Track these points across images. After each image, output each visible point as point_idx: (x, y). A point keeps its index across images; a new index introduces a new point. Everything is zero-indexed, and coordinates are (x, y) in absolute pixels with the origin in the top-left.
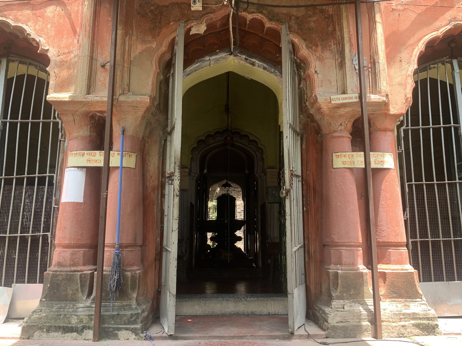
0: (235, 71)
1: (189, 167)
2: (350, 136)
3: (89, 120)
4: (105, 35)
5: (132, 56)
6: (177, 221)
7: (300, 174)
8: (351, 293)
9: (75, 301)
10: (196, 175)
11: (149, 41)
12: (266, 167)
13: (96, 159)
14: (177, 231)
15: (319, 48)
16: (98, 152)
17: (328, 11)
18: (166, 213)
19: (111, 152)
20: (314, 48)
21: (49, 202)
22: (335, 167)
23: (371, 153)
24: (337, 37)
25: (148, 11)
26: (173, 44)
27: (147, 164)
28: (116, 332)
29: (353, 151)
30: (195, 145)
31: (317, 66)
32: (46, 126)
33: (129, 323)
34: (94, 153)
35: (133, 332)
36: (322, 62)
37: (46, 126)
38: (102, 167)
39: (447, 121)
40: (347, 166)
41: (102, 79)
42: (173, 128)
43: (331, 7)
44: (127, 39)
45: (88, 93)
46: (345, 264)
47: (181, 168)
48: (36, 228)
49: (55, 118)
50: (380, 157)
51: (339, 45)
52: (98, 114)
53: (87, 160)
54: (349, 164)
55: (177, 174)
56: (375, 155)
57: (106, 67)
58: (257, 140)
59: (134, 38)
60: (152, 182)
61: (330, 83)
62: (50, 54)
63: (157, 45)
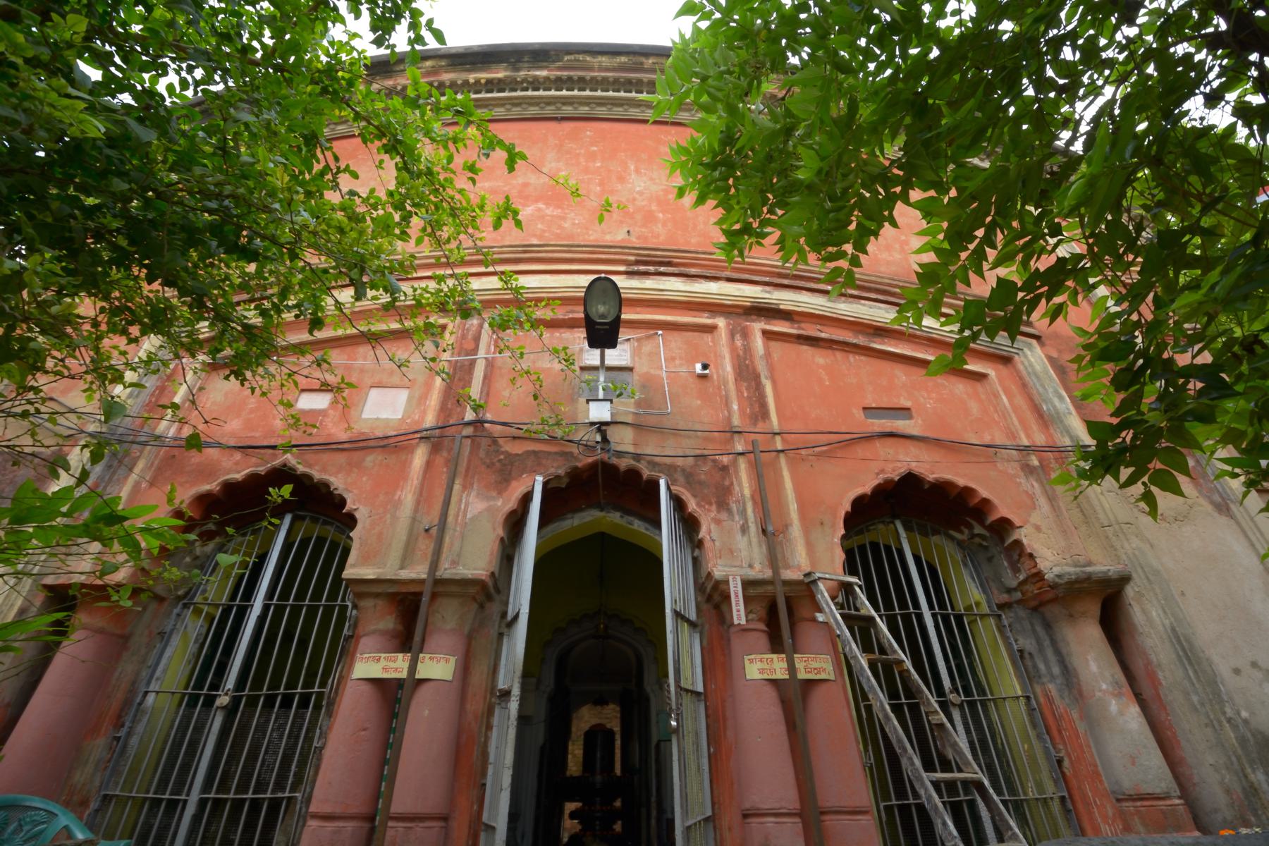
6: (511, 772)
7: (700, 688)
13: (395, 666)
15: (714, 507)
16: (400, 656)
18: (492, 758)
21: (309, 739)
22: (748, 677)
26: (527, 499)
29: (774, 652)
32: (329, 611)
37: (329, 611)
39: (903, 605)
40: (766, 676)
41: (423, 547)
42: (516, 617)
45: (402, 568)
48: (280, 786)
49: (343, 600)
55: (516, 691)
59: (473, 494)
60: (475, 705)
62: (357, 515)
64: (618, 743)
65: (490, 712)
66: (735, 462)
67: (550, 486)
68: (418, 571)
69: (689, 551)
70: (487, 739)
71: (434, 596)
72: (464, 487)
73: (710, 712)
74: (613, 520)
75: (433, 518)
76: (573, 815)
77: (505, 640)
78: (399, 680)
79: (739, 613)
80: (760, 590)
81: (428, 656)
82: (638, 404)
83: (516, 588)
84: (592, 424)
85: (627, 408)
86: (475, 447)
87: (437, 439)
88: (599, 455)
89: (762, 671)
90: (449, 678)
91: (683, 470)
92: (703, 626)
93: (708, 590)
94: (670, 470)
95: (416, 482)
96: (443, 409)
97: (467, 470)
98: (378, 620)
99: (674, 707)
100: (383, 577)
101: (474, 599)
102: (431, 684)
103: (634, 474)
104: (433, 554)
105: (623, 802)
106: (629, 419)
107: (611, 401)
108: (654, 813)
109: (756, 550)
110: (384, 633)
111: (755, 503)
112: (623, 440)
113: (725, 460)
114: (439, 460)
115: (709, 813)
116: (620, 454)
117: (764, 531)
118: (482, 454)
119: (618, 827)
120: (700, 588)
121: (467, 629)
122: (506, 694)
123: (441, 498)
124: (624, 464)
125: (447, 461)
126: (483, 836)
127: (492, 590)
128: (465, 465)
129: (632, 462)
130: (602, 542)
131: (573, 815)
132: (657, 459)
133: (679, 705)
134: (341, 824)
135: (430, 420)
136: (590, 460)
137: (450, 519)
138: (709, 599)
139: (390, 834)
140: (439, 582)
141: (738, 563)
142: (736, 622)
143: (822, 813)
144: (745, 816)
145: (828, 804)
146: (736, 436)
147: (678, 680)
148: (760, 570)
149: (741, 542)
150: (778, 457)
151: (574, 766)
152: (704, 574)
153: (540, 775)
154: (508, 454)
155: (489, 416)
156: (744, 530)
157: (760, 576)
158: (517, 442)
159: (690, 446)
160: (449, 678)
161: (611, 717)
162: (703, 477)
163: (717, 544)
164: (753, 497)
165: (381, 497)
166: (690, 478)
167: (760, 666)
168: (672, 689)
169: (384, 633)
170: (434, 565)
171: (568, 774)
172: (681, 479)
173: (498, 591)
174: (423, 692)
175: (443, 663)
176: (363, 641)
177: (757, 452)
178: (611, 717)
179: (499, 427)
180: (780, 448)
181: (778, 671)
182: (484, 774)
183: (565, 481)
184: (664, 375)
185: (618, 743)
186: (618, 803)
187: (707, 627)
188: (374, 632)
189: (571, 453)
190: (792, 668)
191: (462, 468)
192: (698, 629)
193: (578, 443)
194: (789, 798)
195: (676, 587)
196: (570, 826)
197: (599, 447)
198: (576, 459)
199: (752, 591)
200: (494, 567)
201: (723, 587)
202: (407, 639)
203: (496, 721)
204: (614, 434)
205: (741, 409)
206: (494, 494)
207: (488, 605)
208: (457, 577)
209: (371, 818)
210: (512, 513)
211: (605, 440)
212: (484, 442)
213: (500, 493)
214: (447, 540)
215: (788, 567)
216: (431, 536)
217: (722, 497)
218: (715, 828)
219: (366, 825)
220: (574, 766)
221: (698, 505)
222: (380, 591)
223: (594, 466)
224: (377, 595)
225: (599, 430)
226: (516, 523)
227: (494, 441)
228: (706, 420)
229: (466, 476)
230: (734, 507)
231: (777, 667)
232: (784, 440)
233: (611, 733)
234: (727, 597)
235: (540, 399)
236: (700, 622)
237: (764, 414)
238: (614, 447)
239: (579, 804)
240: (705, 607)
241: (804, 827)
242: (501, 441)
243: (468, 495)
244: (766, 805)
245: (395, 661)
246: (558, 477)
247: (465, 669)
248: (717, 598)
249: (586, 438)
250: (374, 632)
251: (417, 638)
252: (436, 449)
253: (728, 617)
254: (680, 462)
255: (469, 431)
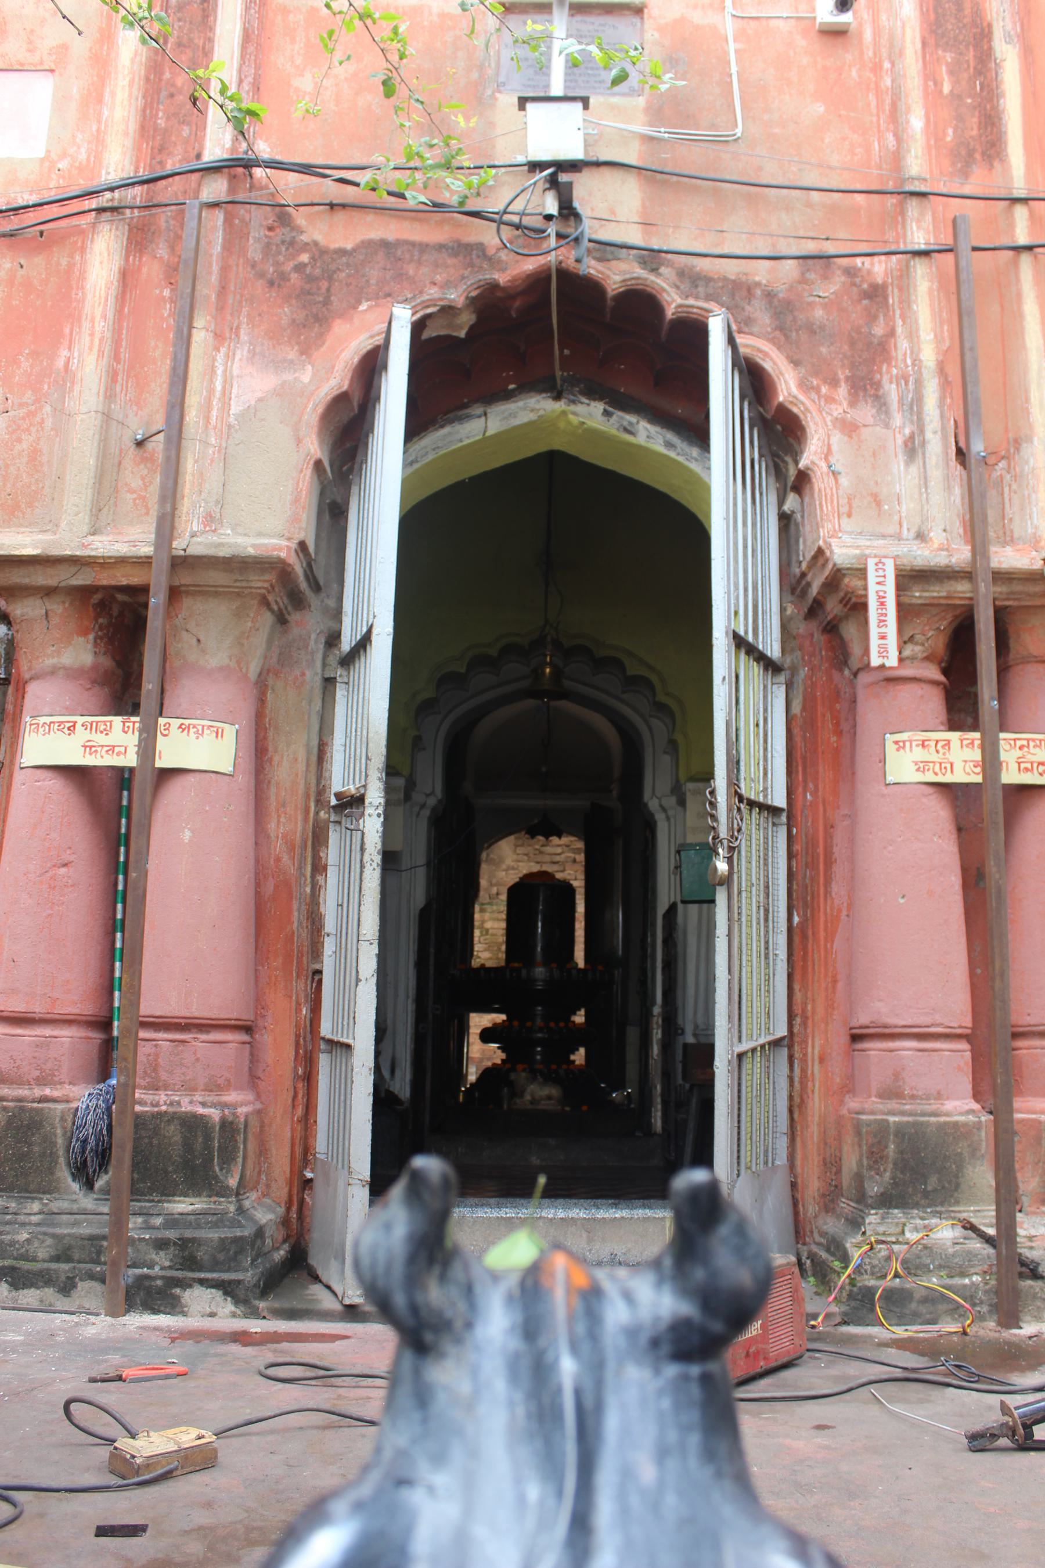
0: (572, 451)
1: (406, 772)
2: (942, 678)
3: (92, 614)
4: (153, 343)
5: (231, 412)
7: (780, 800)
8: (929, 1188)
9: (49, 1192)
10: (432, 802)
11: (291, 362)
12: (682, 777)
13: (111, 742)
14: (374, 980)
16: (117, 720)
17: (869, 272)
18: (330, 924)
19: (162, 721)
20: (824, 390)
22: (890, 779)
23: (1002, 735)
24: (900, 357)
25: (289, 266)
26: (372, 365)
27: (270, 760)
28: (178, 1291)
29: (953, 725)
30: (429, 694)
31: (834, 448)
33: (215, 1266)
34: (105, 722)
35: (226, 1293)
36: (850, 437)
38: (131, 770)
40: (931, 778)
41: (136, 483)
42: (364, 642)
43: (880, 262)
44: (220, 358)
46: (913, 1097)
47: (387, 775)
50: (1037, 750)
51: (907, 383)
52: (120, 597)
53: (85, 747)
54: (937, 769)
55: (375, 796)
56: (1019, 743)
57: (150, 446)
58: (654, 678)
59: (241, 353)
60: (287, 824)
61: (878, 503)
63: (314, 375)
64: (580, 908)
65: (319, 837)
66: (904, 277)
67: (425, 335)
68: (129, 539)
69: (773, 498)
70: (316, 890)
71: (174, 594)
72: (219, 337)
73: (797, 847)
74: (583, 422)
75: (152, 413)
76: (487, 1036)
77: (340, 693)
78: (119, 771)
79: (883, 641)
80: (937, 592)
81: (175, 723)
82: (656, 113)
83: (358, 579)
84: (535, 166)
85: (621, 124)
86: (235, 235)
87: (142, 210)
88: (552, 254)
89: (922, 766)
90: (227, 768)
91: (769, 295)
92: (794, 670)
93: (814, 590)
94: (737, 294)
95: (100, 326)
96: (148, 132)
97: (223, 290)
98: (60, 652)
99: (723, 833)
100: (55, 552)
101: (265, 602)
102: (191, 778)
103: (640, 303)
104: (163, 499)
105: (586, 1016)
106: (631, 158)
107: (585, 102)
108: (657, 1034)
109: (937, 496)
110: (74, 674)
111: (945, 384)
112: (613, 210)
113: (879, 268)
114: (151, 269)
115: (782, 1031)
116: (606, 249)
117: (961, 454)
118: (254, 251)
119: (579, 1057)
120: (793, 585)
121: (253, 669)
122: (352, 803)
123: (165, 366)
124: (615, 276)
125: (171, 273)
126: (324, 1061)
127: (303, 585)
128: (214, 278)
129: (639, 272)
130: (554, 477)
131: (487, 1036)
132: (703, 265)
133: (735, 832)
134: (48, 1031)
135: (117, 162)
136: (530, 265)
137: (192, 415)
138: (814, 610)
139: (144, 1050)
140: (181, 563)
141: (892, 529)
142: (875, 661)
143: (1015, 1036)
144: (856, 1038)
145: (1029, 1020)
146: (913, 204)
147: (733, 783)
148: (944, 547)
149: (902, 478)
150: (1016, 263)
151: (489, 936)
152: (805, 552)
153: (421, 964)
154: (320, 252)
155: (264, 149)
156: (913, 448)
157: (940, 560)
158: (340, 216)
159: (791, 228)
160: (227, 768)
161: (565, 859)
162: (819, 313)
163: (844, 481)
164: (941, 369)
165: (25, 365)
166: (786, 316)
167: (917, 755)
168: (722, 798)
169: (74, 674)
170: (166, 526)
171: (475, 963)
172: (764, 319)
173: (317, 588)
174: (174, 793)
175: (209, 736)
176: (33, 690)
177: (964, 247)
178: (565, 859)
179: (292, 176)
180: (1022, 240)
181: (958, 767)
182: (316, 952)
183: (467, 319)
184: (729, 27)
185: (580, 908)
186: (579, 1018)
187: (803, 672)
188: (53, 672)
189: (481, 247)
190: (991, 762)
191: (208, 289)
192: (782, 678)
193: (498, 220)
194: (955, 1007)
195: (740, 586)
196: (480, 1055)
197: (552, 229)
198: (493, 262)
199: (918, 594)
200: (306, 529)
201: (851, 582)
202: (122, 686)
203: (332, 854)
204: (587, 192)
205: (934, 131)
206: (292, 354)
207: (294, 617)
208: (223, 553)
209: (104, 1024)
210: (340, 400)
211: (568, 211)
212: (257, 219)
213: (305, 351)
214: (189, 466)
215: (1008, 539)
216: (150, 459)
217: (864, 366)
218: (791, 1059)
219: (97, 1036)
220: (489, 936)
221: (802, 384)
222: (52, 582)
223: (539, 281)
224: (49, 592)
225: (553, 183)
226: (348, 428)
227: (282, 215)
228: (835, 160)
229: (221, 308)
230: (892, 391)
231: (960, 758)
232: (1033, 219)
233: (568, 890)
234: (858, 607)
235: (402, 91)
236: (788, 662)
237: (990, 145)
238: (591, 229)
239: (501, 1017)
240: (801, 627)
241: (974, 1059)
242: (300, 218)
243: (229, 357)
244: (900, 1020)
245: (106, 732)
246: (448, 310)
247: (259, 751)
248: (833, 607)
249: (518, 206)
250: (53, 672)
251: (149, 685)
252: (139, 239)
253: (856, 650)
254: (761, 272)
255: (216, 188)
